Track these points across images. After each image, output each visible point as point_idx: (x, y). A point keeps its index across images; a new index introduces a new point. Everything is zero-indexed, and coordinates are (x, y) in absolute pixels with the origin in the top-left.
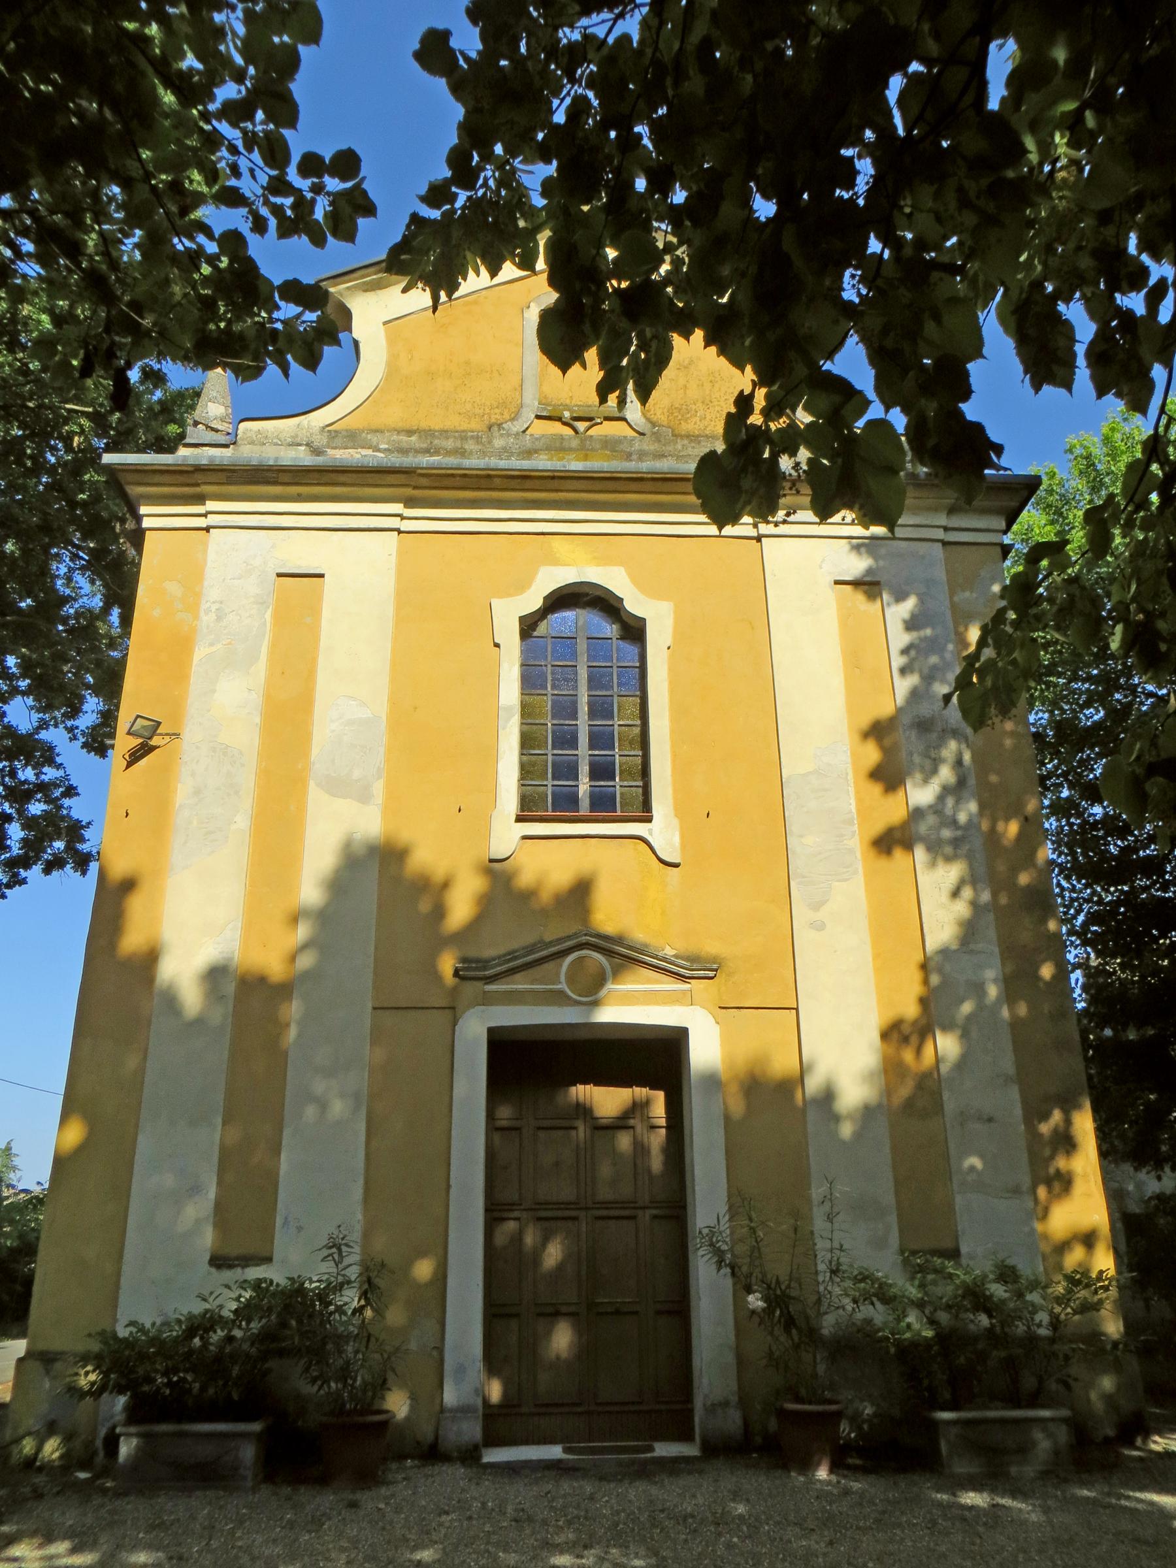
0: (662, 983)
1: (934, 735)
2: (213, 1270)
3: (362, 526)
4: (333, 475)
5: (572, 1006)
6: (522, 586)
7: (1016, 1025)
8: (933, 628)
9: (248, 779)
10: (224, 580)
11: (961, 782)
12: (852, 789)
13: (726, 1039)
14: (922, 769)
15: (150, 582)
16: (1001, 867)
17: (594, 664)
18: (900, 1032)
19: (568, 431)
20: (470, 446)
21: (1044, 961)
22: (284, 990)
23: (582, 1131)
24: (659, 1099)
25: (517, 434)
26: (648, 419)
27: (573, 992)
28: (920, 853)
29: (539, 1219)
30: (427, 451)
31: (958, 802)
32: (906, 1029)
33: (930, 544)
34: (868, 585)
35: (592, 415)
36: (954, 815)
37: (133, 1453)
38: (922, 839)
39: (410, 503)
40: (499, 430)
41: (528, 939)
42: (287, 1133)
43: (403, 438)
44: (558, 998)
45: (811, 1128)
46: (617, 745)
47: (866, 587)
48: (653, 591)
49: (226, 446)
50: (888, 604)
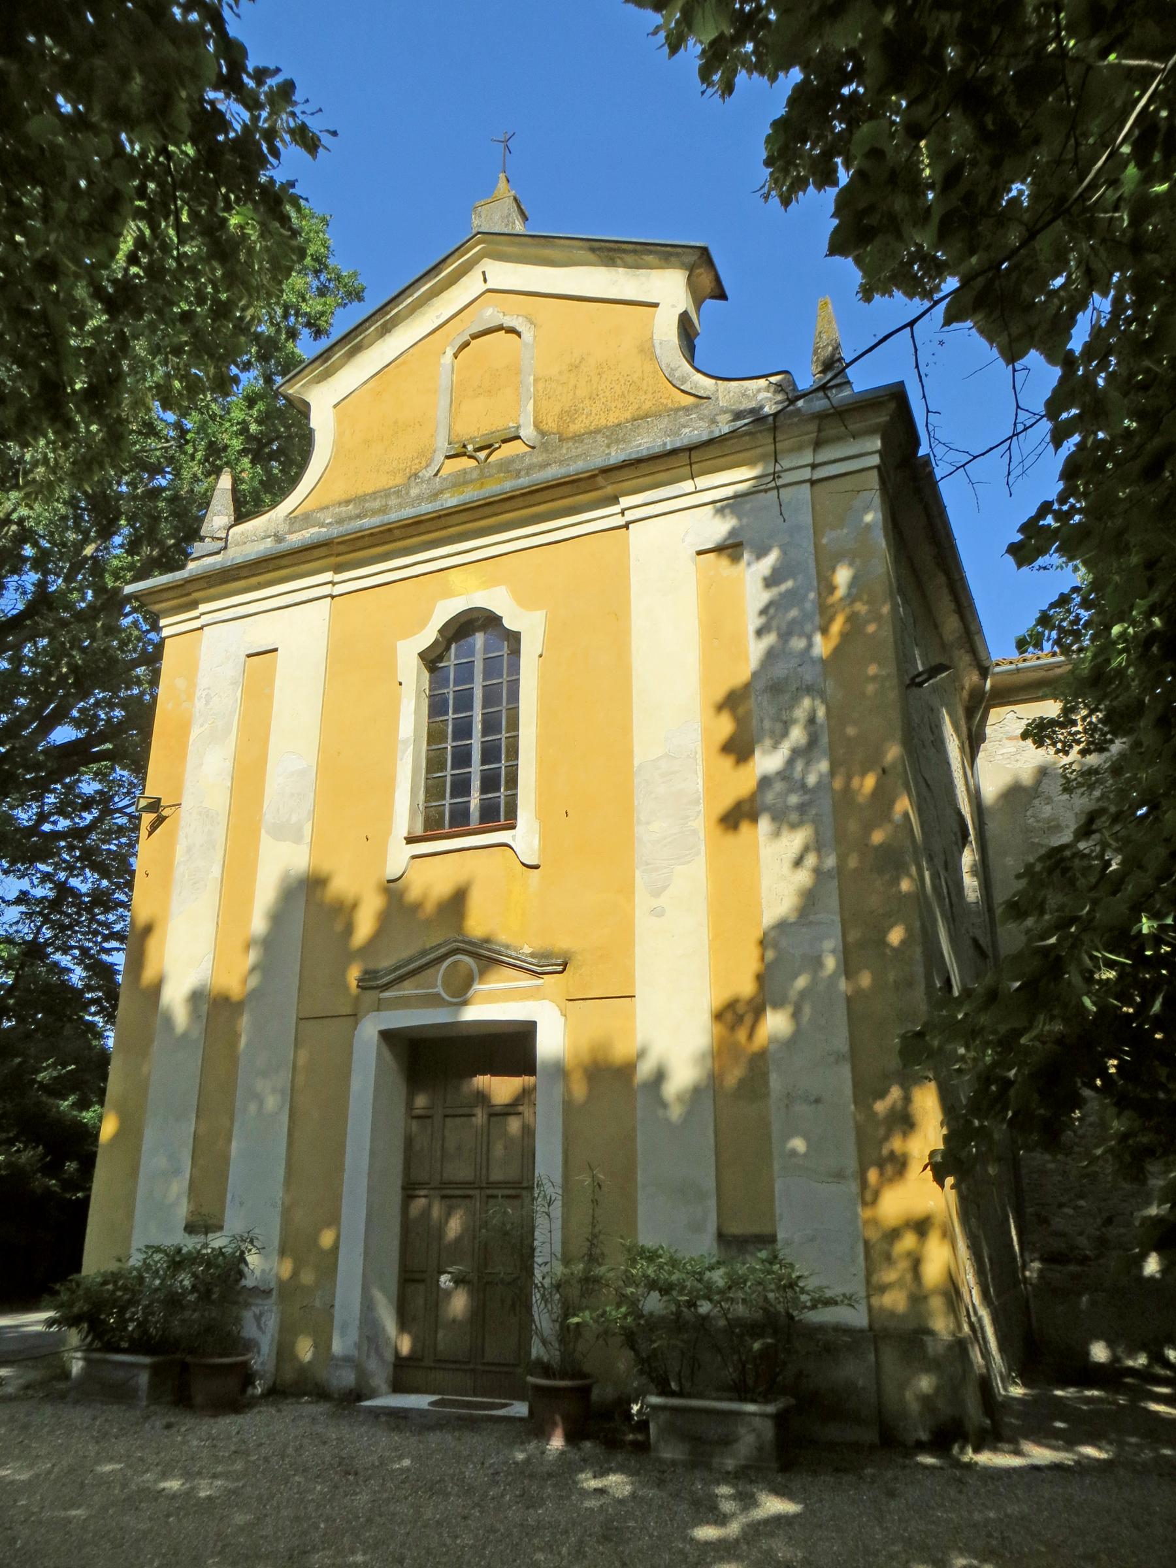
1: (787, 697)
3: (304, 599)
5: (443, 1006)
8: (795, 580)
9: (220, 834)
12: (700, 768)
14: (772, 733)
16: (853, 826)
18: (735, 1013)
23: (480, 1117)
29: (444, 1197)
31: (808, 763)
32: (741, 1008)
33: (796, 487)
34: (730, 549)
36: (803, 778)
39: (338, 569)
42: (237, 1125)
44: (434, 1001)
45: (639, 1114)
47: (730, 551)
49: (218, 553)
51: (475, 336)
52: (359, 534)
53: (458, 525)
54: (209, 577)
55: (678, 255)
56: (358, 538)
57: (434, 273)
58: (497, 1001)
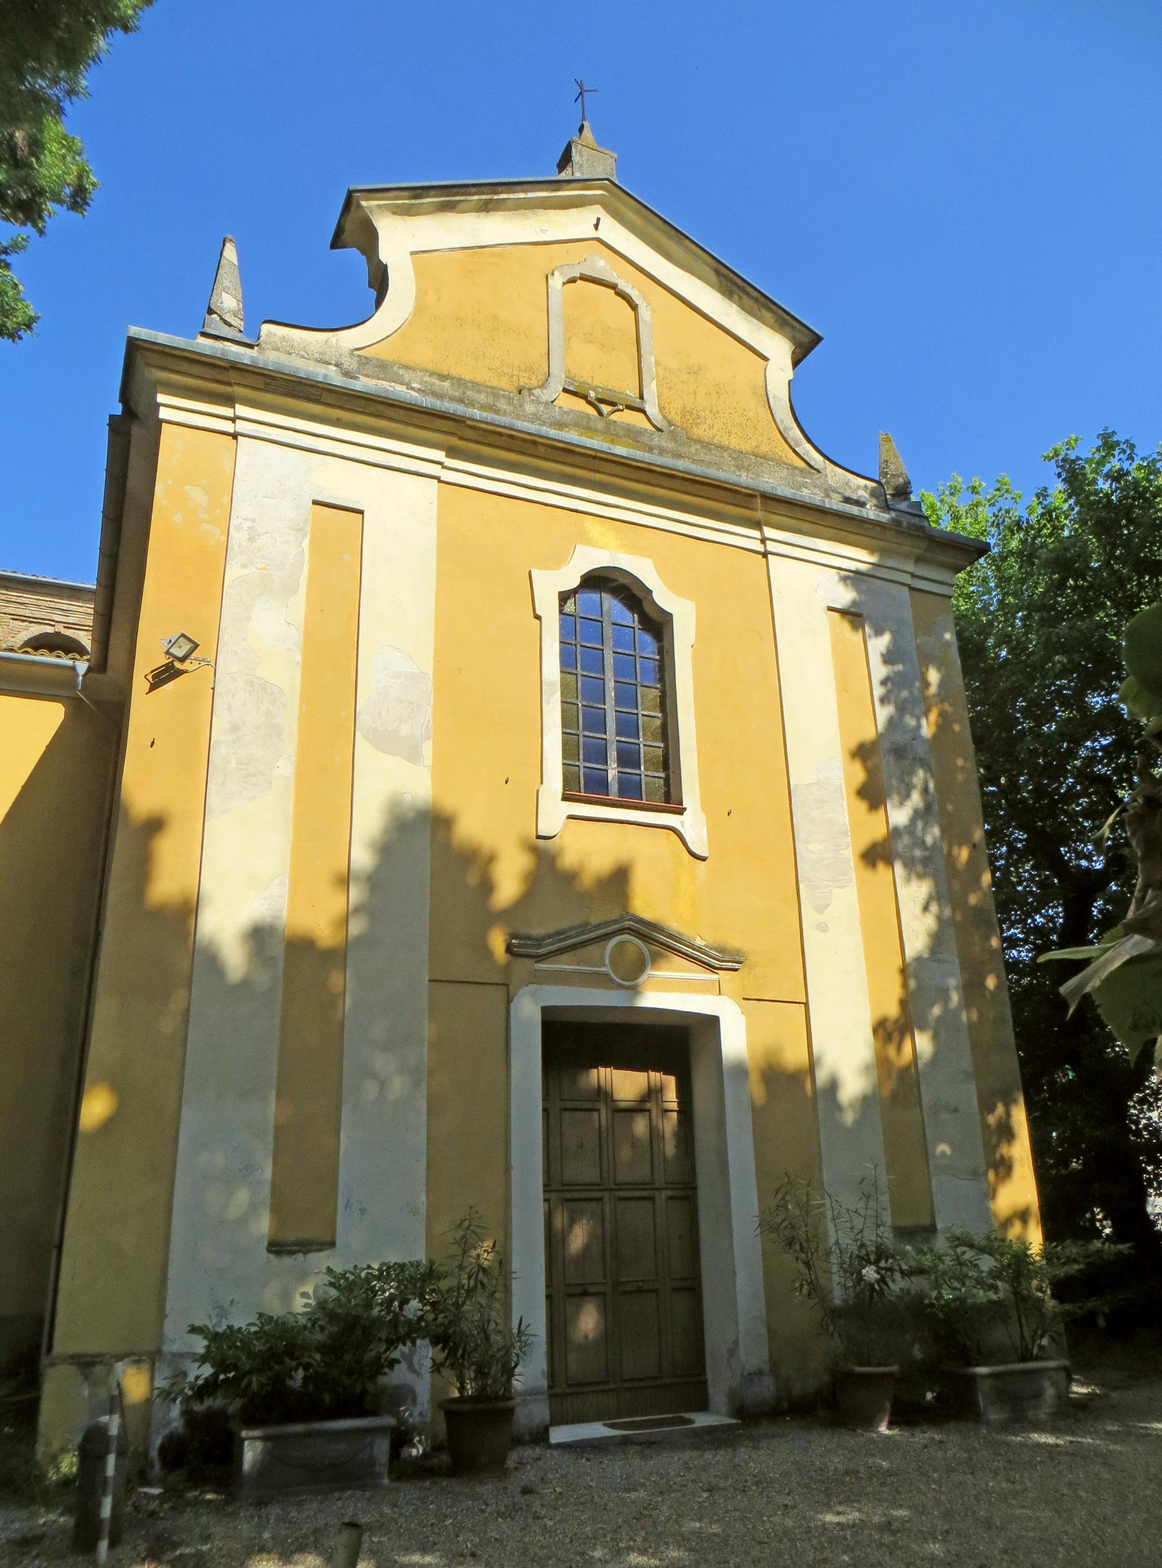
0: (694, 972)
1: (907, 763)
2: (272, 1257)
3: (403, 467)
4: (379, 406)
6: (558, 560)
7: (971, 1026)
9: (290, 720)
10: (255, 497)
11: (928, 807)
12: (845, 804)
13: (751, 1028)
14: (899, 793)
15: (170, 482)
17: (620, 651)
18: (885, 1029)
19: (591, 411)
20: (502, 405)
21: (990, 973)
22: (336, 957)
24: (670, 1082)
25: (546, 403)
26: (664, 417)
27: (616, 975)
28: (899, 868)
30: (461, 401)
31: (926, 825)
35: (615, 401)
37: (260, 1457)
38: (899, 856)
39: (452, 452)
40: (530, 395)
41: (576, 920)
42: (346, 1110)
43: (436, 381)
44: (603, 980)
46: (641, 734)
47: (850, 617)
48: (676, 588)
49: (251, 346)
50: (870, 637)
51: (584, 278)
52: (499, 429)
53: (604, 473)
54: (274, 378)
55: (793, 327)
56: (494, 432)
57: (554, 186)
58: (672, 991)
